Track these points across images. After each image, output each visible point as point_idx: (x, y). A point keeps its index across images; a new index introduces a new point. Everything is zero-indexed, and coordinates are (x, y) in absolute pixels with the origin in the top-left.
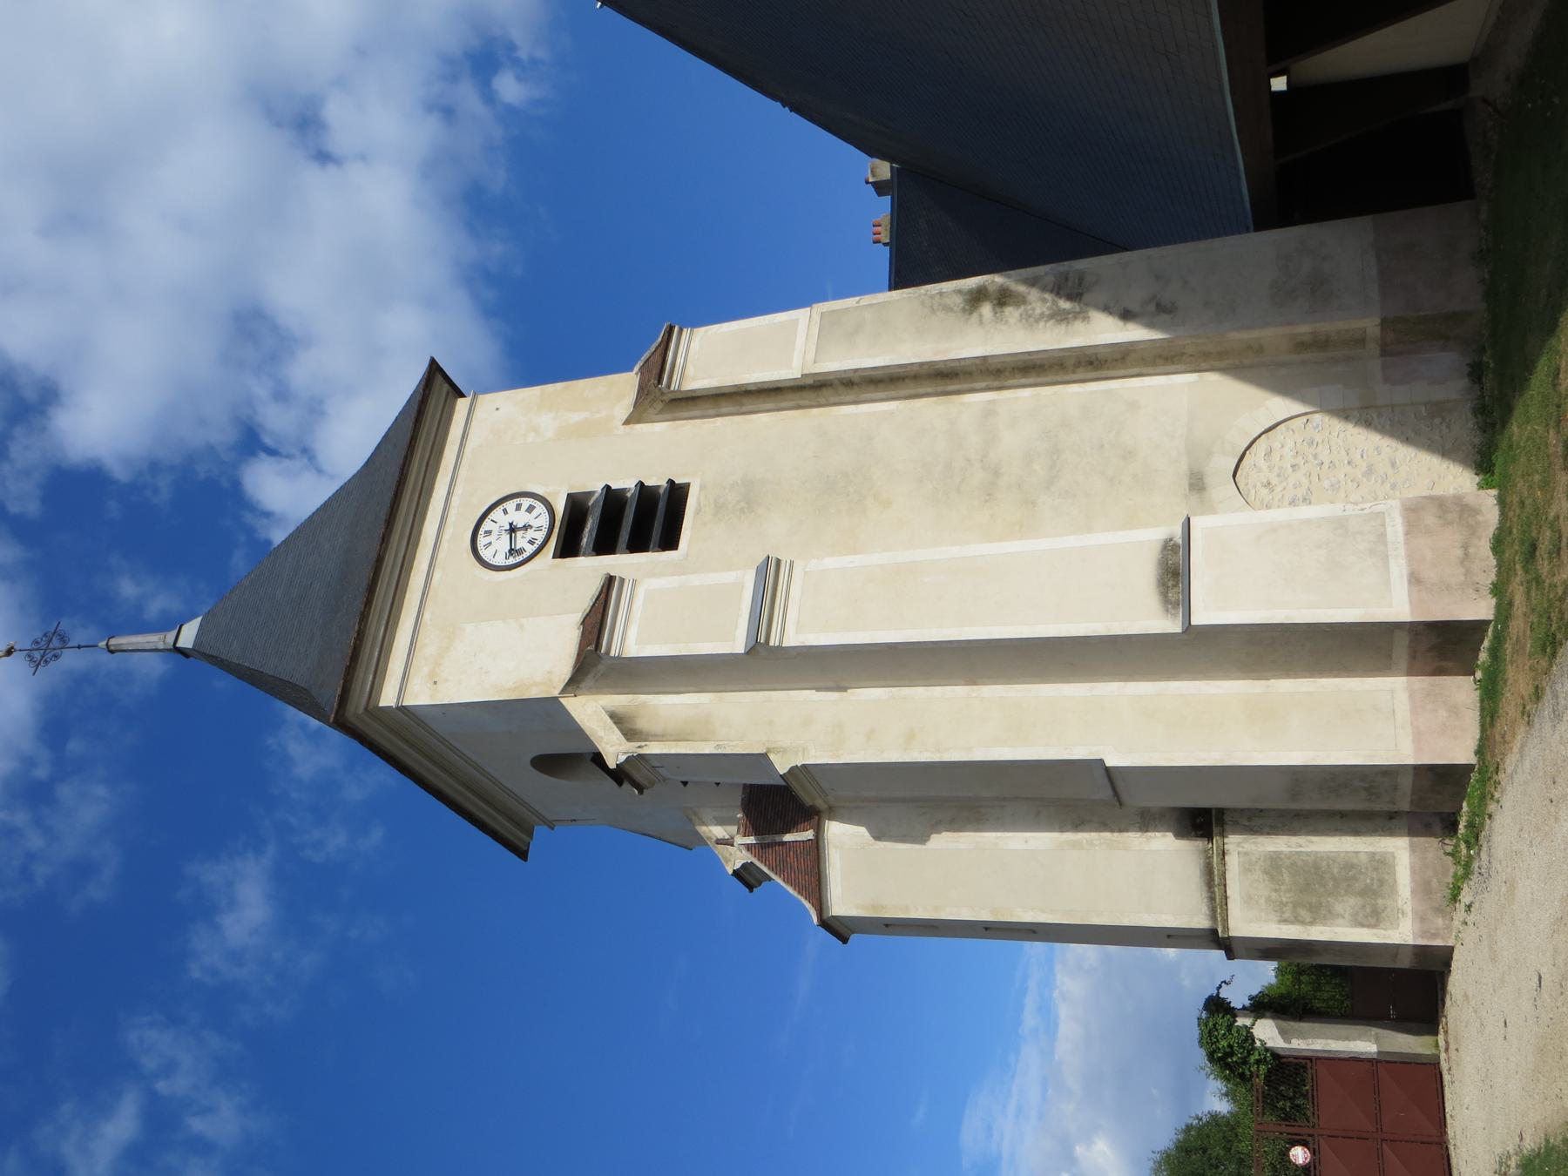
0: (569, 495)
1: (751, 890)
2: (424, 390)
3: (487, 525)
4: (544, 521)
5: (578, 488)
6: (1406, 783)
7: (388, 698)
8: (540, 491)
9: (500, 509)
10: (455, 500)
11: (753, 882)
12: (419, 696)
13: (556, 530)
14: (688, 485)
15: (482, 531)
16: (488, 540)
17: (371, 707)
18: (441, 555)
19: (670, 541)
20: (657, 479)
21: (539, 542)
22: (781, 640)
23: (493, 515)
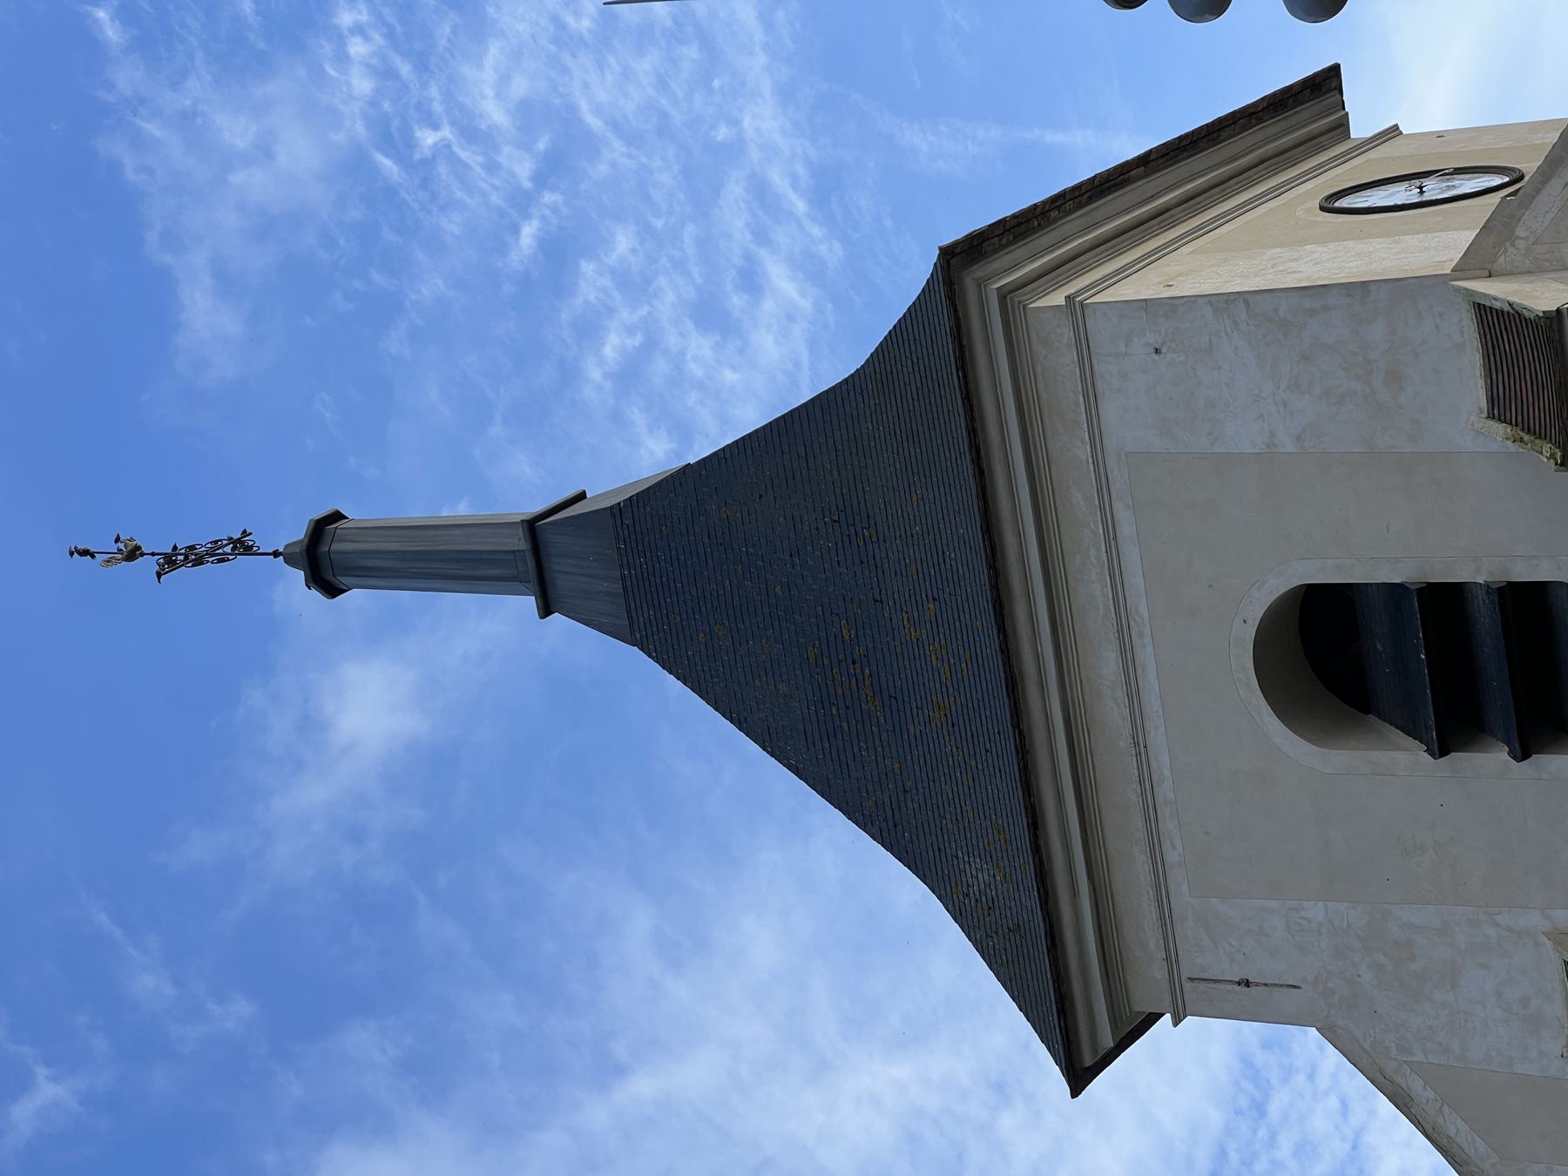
17: (1019, 296)
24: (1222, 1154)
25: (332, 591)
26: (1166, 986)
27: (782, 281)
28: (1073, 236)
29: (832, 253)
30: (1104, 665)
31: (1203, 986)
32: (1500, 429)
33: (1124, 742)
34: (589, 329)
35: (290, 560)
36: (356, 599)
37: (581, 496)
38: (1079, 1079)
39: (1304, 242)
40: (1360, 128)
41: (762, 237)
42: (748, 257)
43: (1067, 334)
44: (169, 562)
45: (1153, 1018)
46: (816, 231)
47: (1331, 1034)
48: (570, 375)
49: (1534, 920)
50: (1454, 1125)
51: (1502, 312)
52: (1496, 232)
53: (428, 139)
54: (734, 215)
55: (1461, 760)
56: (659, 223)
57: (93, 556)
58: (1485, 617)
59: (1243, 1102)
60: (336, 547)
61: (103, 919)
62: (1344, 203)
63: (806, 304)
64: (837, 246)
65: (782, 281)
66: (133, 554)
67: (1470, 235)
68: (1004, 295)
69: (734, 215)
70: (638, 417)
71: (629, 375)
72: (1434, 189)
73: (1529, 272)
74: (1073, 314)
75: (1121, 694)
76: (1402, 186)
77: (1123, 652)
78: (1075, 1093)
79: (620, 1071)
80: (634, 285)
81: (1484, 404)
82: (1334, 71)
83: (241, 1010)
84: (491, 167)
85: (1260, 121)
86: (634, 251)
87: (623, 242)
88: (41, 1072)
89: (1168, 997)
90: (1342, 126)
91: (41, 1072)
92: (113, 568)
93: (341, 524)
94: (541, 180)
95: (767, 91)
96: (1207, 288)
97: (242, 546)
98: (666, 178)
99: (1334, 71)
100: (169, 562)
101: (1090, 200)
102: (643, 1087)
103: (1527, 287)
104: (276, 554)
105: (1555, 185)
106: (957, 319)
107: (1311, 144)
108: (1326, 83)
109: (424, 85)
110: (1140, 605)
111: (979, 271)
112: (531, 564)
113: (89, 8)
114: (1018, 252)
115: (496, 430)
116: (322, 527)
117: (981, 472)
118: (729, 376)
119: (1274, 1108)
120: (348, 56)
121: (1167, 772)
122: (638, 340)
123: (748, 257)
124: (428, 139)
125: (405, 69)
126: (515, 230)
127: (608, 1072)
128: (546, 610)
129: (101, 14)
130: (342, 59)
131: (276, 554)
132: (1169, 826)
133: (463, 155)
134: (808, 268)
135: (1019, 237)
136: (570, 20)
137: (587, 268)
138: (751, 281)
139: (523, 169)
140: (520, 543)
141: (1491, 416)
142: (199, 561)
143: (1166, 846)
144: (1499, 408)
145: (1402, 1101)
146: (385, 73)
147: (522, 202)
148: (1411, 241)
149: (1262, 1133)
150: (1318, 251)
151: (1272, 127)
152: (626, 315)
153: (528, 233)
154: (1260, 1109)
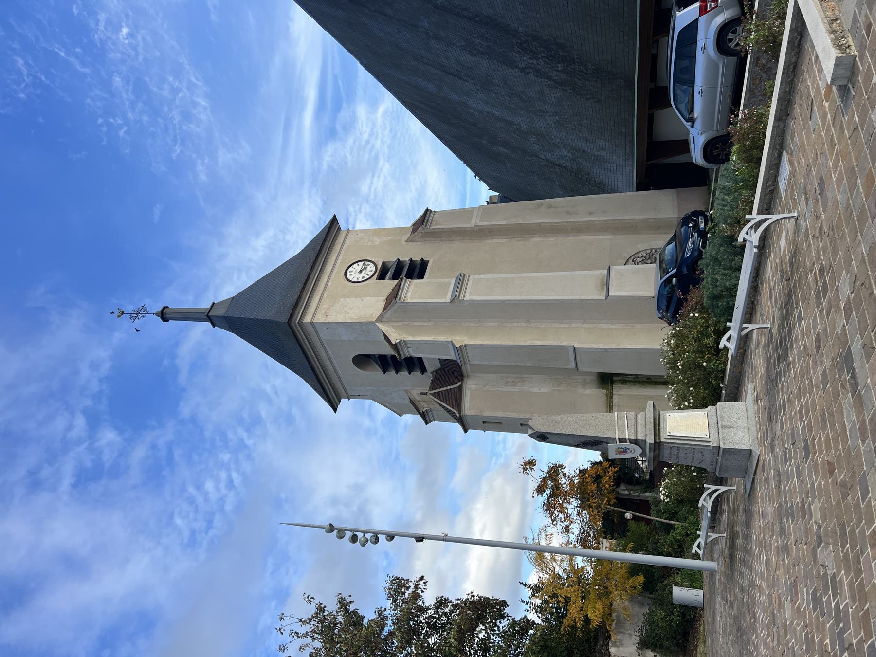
0: (383, 262)
1: (466, 431)
2: (331, 224)
3: (351, 269)
4: (373, 268)
5: (386, 260)
6: (651, 188)
7: (307, 319)
8: (372, 260)
9: (356, 265)
10: (339, 261)
11: (429, 421)
12: (320, 319)
13: (378, 272)
14: (428, 261)
15: (349, 270)
16: (351, 273)
18: (333, 277)
19: (421, 276)
20: (417, 259)
21: (365, 279)
22: (464, 298)
23: (353, 266)
35: (157, 314)
43: (311, 326)
49: (402, 388)
104: (154, 314)
131: (154, 314)
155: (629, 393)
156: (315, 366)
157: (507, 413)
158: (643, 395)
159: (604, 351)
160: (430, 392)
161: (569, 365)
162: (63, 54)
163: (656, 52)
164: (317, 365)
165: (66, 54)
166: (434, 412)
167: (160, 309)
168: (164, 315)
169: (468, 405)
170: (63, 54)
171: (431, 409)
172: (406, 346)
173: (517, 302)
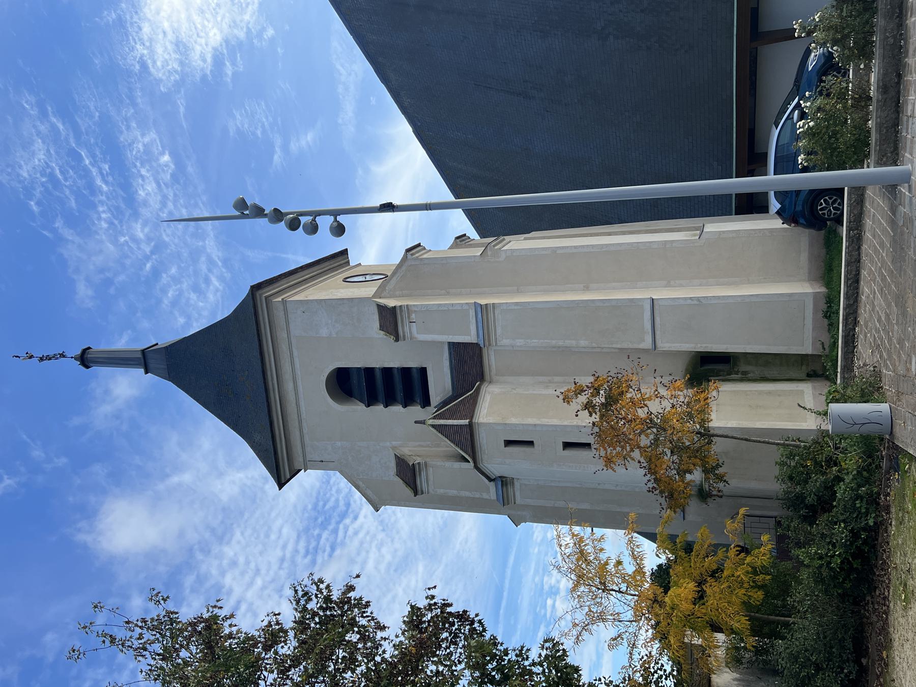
17: (270, 298)
24: (319, 493)
25: (87, 367)
26: (303, 463)
27: (215, 282)
28: (284, 284)
29: (228, 275)
30: (289, 386)
31: (312, 462)
32: (382, 333)
33: (294, 405)
34: (164, 291)
35: (76, 359)
36: (94, 369)
37: (157, 344)
38: (281, 485)
39: (339, 288)
40: (352, 264)
41: (210, 270)
42: (206, 275)
43: (282, 307)
44: (41, 359)
45: (300, 470)
46: (224, 270)
47: (341, 472)
48: (159, 302)
49: (388, 444)
50: (369, 492)
51: (382, 306)
52: (382, 288)
53: (122, 239)
54: (203, 267)
55: (373, 408)
56: (183, 265)
57: (19, 357)
58: (378, 375)
59: (324, 480)
60: (89, 356)
61: (25, 437)
62: (348, 280)
63: (221, 288)
64: (229, 274)
65: (215, 282)
66: (31, 357)
67: (376, 288)
68: (266, 298)
69: (203, 267)
70: (177, 313)
71: (174, 303)
72: (368, 278)
73: (388, 298)
74: (284, 304)
75: (293, 393)
76: (361, 277)
77: (294, 383)
78: (280, 489)
79: (168, 476)
80: (176, 280)
81: (379, 327)
82: (346, 250)
83: (62, 461)
84: (139, 248)
85: (329, 260)
86: (176, 272)
87: (173, 270)
88: (5, 477)
89: (303, 466)
90: (348, 262)
91: (5, 477)
92: (25, 361)
93: (91, 350)
94: (152, 252)
95: (212, 236)
96: (316, 298)
97: (62, 355)
98: (185, 255)
99: (346, 250)
100: (41, 359)
101: (288, 276)
102: (175, 479)
103: (388, 301)
104: (72, 357)
105: (394, 278)
106: (254, 303)
107: (341, 266)
108: (344, 253)
109: (121, 226)
110: (298, 372)
111: (260, 292)
112: (143, 361)
113: (28, 201)
114: (271, 287)
115: (139, 314)
116: (84, 351)
117: (260, 340)
118: (201, 304)
119: (332, 482)
120: (101, 218)
121: (304, 412)
122: (177, 293)
123: (206, 275)
124: (122, 239)
125: (116, 222)
126: (145, 265)
127: (165, 476)
128: (146, 372)
129: (32, 203)
130: (99, 219)
131: (72, 357)
132: (304, 424)
133: (132, 245)
134: (221, 278)
135: (270, 284)
136: (161, 214)
137: (164, 275)
138: (207, 281)
139: (148, 250)
140: (140, 355)
141: (380, 330)
142: (50, 359)
143: (304, 430)
144: (382, 328)
145: (357, 488)
146: (111, 223)
147: (147, 258)
148: (363, 289)
149: (329, 487)
150: (342, 291)
151: (332, 262)
152: (174, 287)
153: (148, 266)
154: (328, 482)
155: (735, 389)
156: (272, 398)
157: (543, 420)
158: (755, 391)
159: (695, 302)
160: (431, 422)
161: (644, 341)
162: (87, 162)
163: (756, 6)
164: (273, 384)
165: (91, 163)
166: (431, 470)
167: (79, 352)
168: (85, 359)
169: (486, 411)
170: (87, 162)
171: (426, 463)
172: (409, 317)
173: (574, 251)
